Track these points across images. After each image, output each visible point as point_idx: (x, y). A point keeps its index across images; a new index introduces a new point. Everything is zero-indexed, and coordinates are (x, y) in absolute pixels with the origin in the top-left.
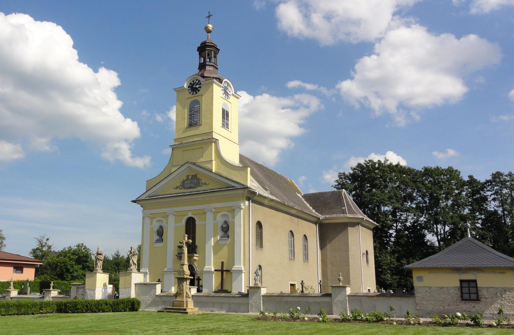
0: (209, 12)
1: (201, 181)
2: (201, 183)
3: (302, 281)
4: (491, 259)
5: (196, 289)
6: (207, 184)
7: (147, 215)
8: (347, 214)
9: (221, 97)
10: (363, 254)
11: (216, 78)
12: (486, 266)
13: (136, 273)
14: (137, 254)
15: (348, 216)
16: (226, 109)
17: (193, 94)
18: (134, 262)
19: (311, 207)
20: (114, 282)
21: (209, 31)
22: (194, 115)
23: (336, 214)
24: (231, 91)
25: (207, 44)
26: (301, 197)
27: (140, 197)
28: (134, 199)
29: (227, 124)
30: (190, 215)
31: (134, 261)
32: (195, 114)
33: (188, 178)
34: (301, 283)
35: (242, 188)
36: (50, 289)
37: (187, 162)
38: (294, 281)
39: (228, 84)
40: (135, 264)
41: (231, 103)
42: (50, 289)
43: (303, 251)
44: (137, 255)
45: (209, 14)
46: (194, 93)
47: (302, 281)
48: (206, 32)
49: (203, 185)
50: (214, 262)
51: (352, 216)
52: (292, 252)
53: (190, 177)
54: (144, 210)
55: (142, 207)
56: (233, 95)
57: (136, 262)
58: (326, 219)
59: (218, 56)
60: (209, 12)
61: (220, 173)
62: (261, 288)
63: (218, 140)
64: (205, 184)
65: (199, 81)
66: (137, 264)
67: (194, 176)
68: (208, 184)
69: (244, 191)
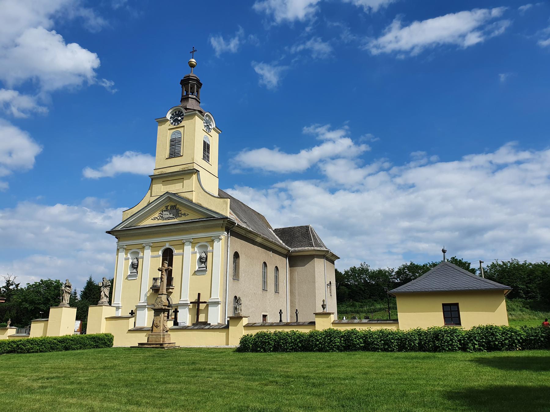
0: (193, 48)
1: (180, 212)
2: (180, 214)
3: (281, 310)
4: (471, 282)
5: (173, 321)
6: (187, 214)
7: (121, 247)
8: (313, 246)
9: (203, 130)
10: (328, 285)
11: (199, 111)
12: (467, 288)
13: (107, 306)
14: (110, 285)
15: (316, 248)
16: (208, 142)
17: (175, 125)
18: (105, 294)
19: (282, 241)
20: (82, 316)
21: (192, 66)
22: (176, 146)
23: (304, 247)
24: (212, 125)
25: (190, 77)
26: (272, 232)
27: (116, 228)
28: (109, 230)
29: (208, 157)
30: (167, 246)
31: (106, 293)
32: (173, 156)
33: (167, 208)
34: (280, 313)
35: (222, 218)
36: (7, 328)
37: (167, 192)
38: (266, 312)
39: (210, 118)
40: (107, 297)
41: (212, 137)
42: (7, 328)
43: (275, 282)
44: (109, 286)
45: (193, 49)
46: (176, 124)
47: (281, 310)
48: (190, 66)
49: (182, 216)
50: (190, 294)
51: (319, 249)
52: (265, 282)
53: (169, 208)
54: (119, 241)
55: (117, 238)
56: (214, 129)
57: (107, 294)
58: (295, 251)
59: (201, 91)
60: (193, 48)
61: (200, 204)
62: (243, 318)
63: (199, 171)
64: (184, 214)
65: (182, 112)
66: (108, 297)
67: (173, 206)
68: (188, 215)
69: (224, 221)
